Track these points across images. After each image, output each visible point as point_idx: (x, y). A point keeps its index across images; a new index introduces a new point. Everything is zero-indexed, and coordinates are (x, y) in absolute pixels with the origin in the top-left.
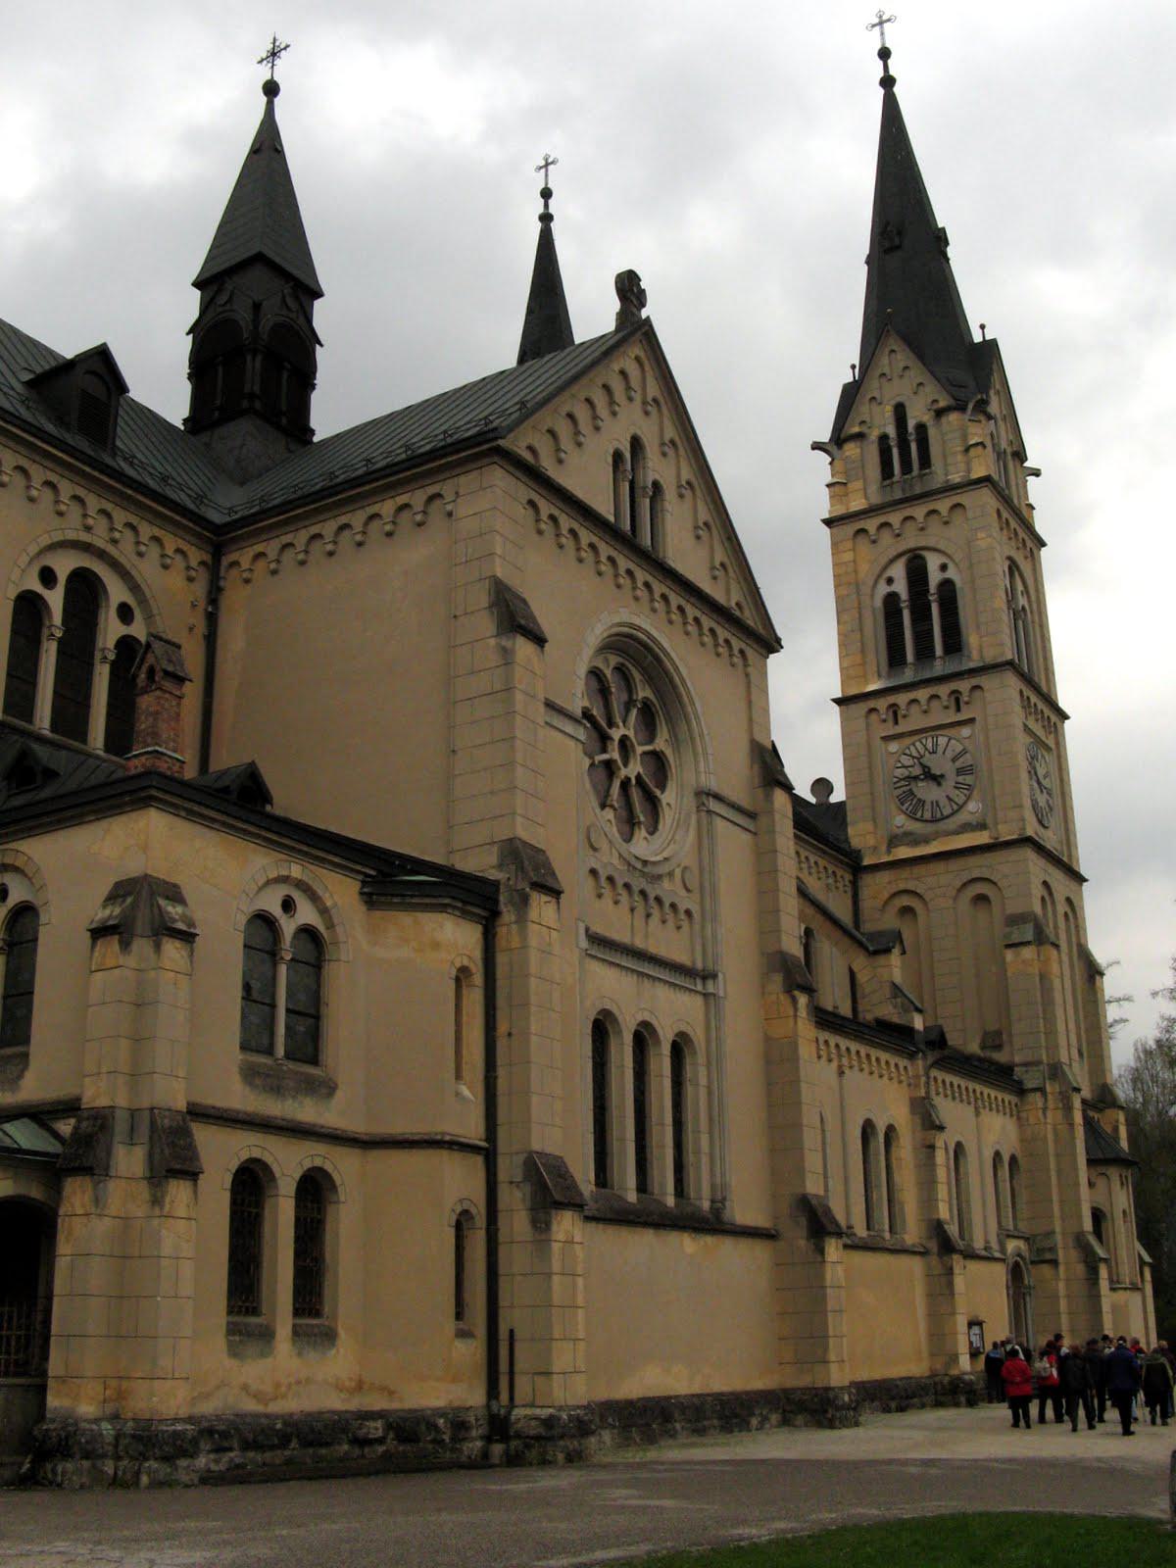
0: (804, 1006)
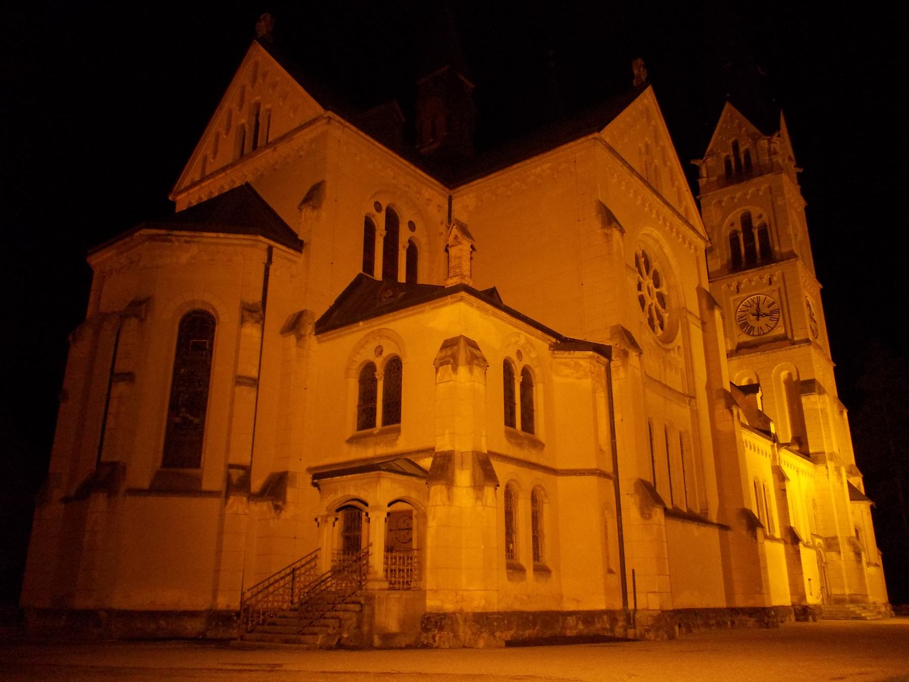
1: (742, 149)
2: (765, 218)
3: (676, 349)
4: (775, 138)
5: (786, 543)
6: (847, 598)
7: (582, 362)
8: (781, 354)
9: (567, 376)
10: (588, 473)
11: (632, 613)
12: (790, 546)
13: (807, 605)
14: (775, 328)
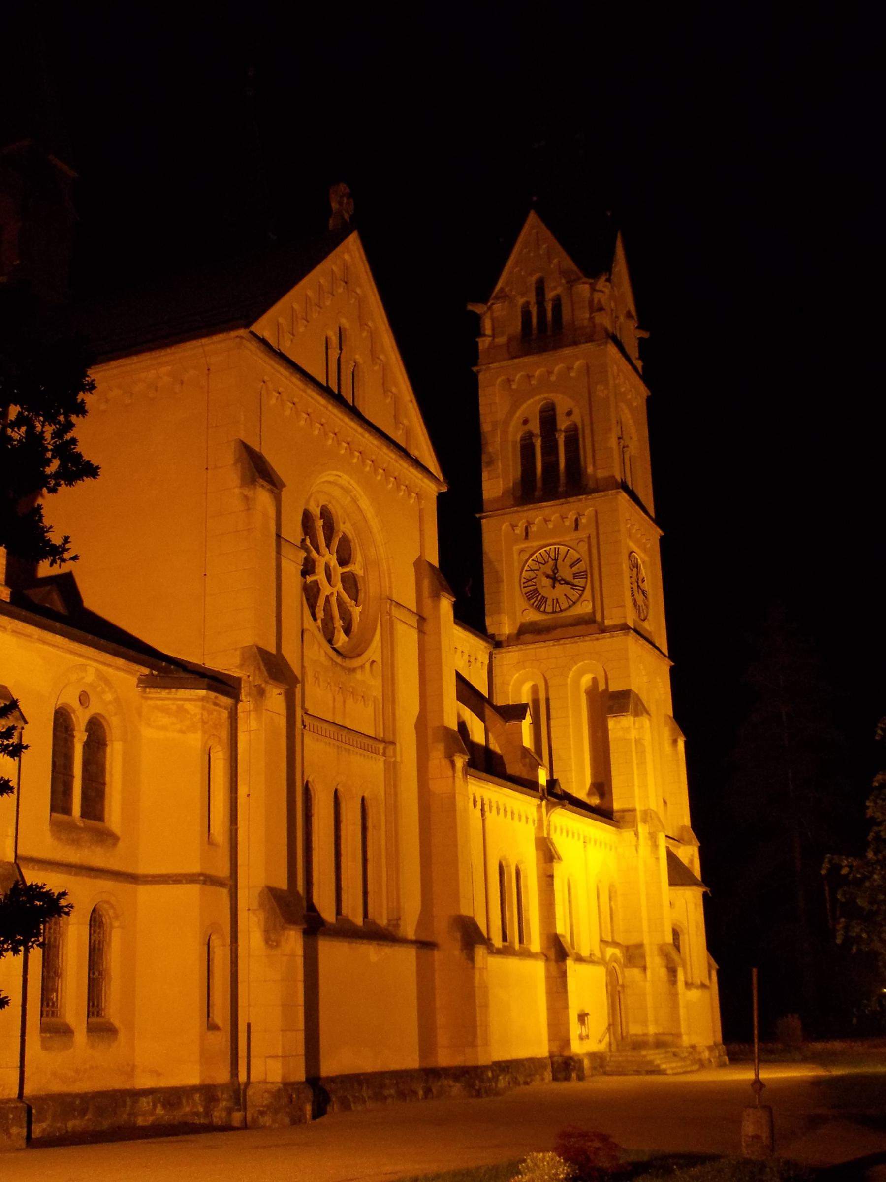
0: (460, 769)
1: (550, 295)
2: (576, 417)
3: (368, 665)
4: (601, 283)
5: (547, 959)
6: (651, 1039)
7: (188, 706)
8: (586, 645)
9: (164, 728)
10: (186, 880)
11: (242, 1087)
12: (553, 965)
13: (572, 1055)
14: (579, 603)
